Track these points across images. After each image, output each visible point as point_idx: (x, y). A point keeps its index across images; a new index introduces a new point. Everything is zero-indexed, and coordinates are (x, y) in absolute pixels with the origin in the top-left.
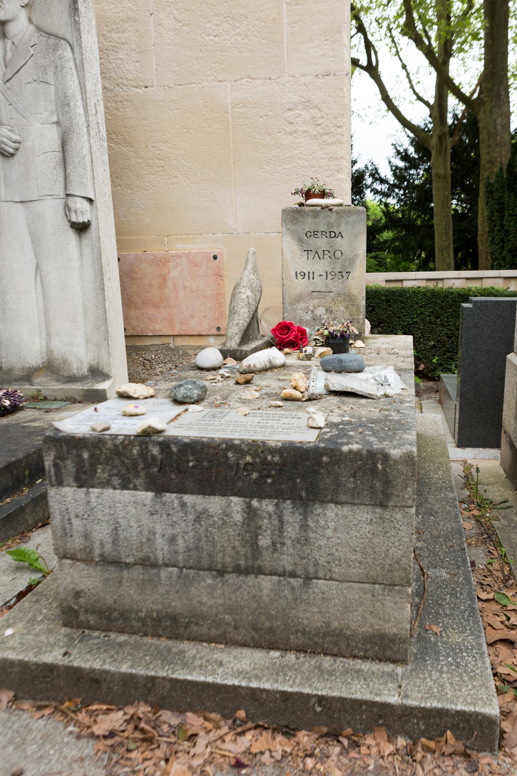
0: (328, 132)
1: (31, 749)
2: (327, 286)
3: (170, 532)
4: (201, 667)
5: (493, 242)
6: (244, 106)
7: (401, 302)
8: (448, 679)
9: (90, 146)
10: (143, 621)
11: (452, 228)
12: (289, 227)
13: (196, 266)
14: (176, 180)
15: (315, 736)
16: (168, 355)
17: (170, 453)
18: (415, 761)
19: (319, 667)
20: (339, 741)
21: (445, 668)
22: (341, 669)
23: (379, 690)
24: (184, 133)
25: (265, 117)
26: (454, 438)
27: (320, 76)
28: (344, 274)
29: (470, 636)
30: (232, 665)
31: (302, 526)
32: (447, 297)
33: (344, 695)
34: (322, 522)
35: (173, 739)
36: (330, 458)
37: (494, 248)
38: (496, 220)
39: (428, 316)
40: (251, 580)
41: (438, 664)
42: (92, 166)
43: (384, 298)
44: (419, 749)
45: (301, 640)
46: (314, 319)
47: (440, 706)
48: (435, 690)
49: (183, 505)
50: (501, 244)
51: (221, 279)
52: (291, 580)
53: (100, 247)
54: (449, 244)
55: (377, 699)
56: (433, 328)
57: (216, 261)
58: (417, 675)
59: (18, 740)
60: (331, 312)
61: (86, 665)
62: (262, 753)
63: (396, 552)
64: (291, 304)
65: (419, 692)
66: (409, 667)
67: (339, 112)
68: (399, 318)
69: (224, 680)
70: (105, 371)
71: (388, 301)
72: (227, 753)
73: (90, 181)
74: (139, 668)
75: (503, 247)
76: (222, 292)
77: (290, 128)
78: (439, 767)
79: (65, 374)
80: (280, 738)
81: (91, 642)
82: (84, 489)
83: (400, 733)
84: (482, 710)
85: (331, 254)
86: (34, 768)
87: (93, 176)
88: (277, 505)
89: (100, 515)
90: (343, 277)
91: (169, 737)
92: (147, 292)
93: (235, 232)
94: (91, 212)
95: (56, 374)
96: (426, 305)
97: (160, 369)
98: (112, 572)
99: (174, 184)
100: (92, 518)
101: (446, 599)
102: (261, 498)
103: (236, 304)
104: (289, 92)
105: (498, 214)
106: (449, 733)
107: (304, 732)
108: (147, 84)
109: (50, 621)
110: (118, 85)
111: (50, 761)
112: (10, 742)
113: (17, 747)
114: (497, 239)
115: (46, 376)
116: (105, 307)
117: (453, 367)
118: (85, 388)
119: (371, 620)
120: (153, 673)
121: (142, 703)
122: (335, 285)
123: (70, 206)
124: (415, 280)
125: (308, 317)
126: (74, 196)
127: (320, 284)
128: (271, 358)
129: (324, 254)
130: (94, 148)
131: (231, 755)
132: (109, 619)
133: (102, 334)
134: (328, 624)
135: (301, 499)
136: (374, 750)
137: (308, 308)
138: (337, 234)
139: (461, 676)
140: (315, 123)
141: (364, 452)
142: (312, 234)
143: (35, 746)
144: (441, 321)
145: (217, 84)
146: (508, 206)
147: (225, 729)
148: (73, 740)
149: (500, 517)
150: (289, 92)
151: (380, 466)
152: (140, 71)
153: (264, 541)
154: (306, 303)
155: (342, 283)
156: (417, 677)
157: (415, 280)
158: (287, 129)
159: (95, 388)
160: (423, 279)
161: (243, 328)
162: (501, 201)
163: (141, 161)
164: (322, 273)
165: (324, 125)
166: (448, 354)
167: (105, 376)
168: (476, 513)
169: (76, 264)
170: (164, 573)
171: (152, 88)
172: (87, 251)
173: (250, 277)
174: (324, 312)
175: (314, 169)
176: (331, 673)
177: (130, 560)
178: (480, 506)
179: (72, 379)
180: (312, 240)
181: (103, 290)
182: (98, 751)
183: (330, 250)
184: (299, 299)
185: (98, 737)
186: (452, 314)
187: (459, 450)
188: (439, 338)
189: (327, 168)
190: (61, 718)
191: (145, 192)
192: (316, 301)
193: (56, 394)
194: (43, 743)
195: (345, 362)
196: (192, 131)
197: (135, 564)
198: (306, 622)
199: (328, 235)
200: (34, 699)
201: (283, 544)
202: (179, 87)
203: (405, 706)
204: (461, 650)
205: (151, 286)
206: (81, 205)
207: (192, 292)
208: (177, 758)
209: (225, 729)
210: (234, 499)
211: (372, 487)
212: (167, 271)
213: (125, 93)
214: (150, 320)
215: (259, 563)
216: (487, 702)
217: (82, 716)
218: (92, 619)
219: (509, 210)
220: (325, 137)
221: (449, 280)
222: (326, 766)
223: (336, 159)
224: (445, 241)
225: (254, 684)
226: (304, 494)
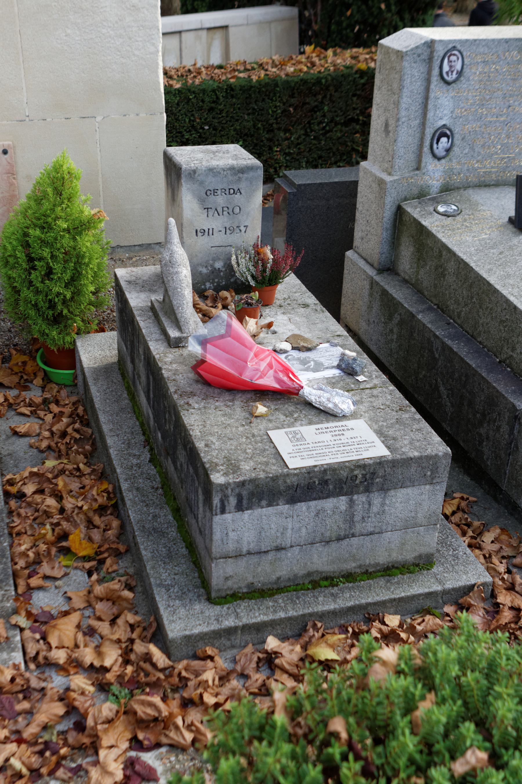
51: (14, 178)
57: (6, 156)
85: (230, 211)
90: (240, 231)
93: (27, 119)
129: (223, 211)
138: (236, 191)
142: (212, 192)
180: (212, 197)
183: (229, 206)
199: (227, 192)
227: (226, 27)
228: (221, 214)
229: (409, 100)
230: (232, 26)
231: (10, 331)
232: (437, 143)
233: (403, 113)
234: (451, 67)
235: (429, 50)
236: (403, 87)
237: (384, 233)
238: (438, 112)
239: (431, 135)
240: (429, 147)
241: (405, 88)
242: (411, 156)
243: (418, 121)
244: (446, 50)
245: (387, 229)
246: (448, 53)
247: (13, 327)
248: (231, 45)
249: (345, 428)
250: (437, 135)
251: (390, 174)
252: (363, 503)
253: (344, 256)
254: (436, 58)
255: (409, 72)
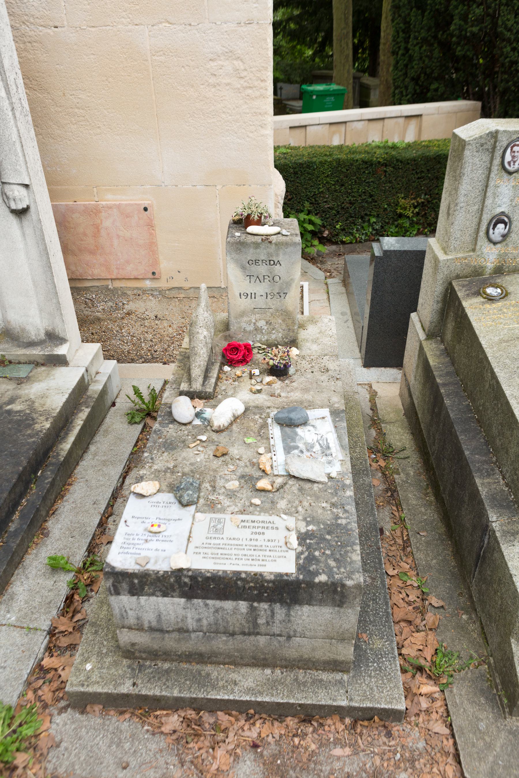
0: (251, 86)
1: (127, 746)
2: (267, 304)
3: (197, 617)
4: (223, 686)
5: (396, 67)
6: (164, 54)
7: (308, 173)
8: (376, 682)
9: (18, 130)
10: (179, 656)
11: (351, 9)
12: (233, 256)
13: (127, 217)
14: (99, 131)
15: (296, 720)
16: (108, 295)
17: (198, 582)
18: (356, 733)
19: (296, 680)
20: (312, 724)
21: (373, 674)
22: (310, 680)
23: (335, 696)
24: (103, 81)
25: (186, 67)
26: (360, 352)
27: (242, 24)
28: (282, 294)
29: (386, 642)
30: (243, 683)
31: (286, 615)
32: (352, 165)
33: (314, 703)
34: (300, 613)
35: (213, 733)
36: (307, 585)
37: (397, 74)
38: (401, 42)
39: (333, 185)
40: (252, 638)
41: (368, 670)
42: (23, 150)
43: (292, 171)
44: (359, 726)
45: (284, 663)
46: (256, 330)
47: (371, 705)
48: (368, 693)
49: (206, 605)
50: (404, 71)
52: (279, 638)
53: (41, 228)
54: (348, 33)
55: (335, 704)
56: (337, 196)
58: (357, 680)
59: (116, 740)
60: (270, 324)
61: (151, 693)
62: (268, 736)
63: (346, 626)
64: (236, 318)
65: (359, 695)
66: (351, 675)
67: (263, 65)
68: (306, 189)
69: (241, 697)
70: (61, 335)
71: (295, 173)
72: (247, 739)
73: (24, 167)
74: (185, 692)
75: (406, 74)
76: (155, 241)
77: (212, 80)
78: (370, 736)
79: (25, 341)
80: (276, 724)
81: (147, 671)
82: (136, 597)
83: (346, 716)
84: (396, 707)
85: (271, 279)
86: (134, 760)
87: (26, 161)
88: (270, 605)
89: (147, 609)
91: (210, 731)
92: (82, 240)
94: (29, 196)
95: (16, 340)
96: (332, 174)
97: (101, 307)
98: (157, 635)
99: (97, 134)
100: (142, 610)
101: (370, 606)
102: (259, 602)
103: (195, 345)
104: (210, 40)
105: (404, 35)
106: (376, 717)
107: (289, 718)
108: (57, 24)
109: (113, 653)
110: (23, 23)
111: (142, 754)
112: (112, 743)
113: (118, 746)
114: (401, 63)
115: (7, 342)
116: (54, 283)
117: (355, 231)
118: (46, 353)
119: (328, 654)
120: (195, 696)
121: (188, 708)
122: (274, 303)
123: (7, 194)
124: (319, 124)
125: (251, 328)
126: (9, 184)
127: (261, 302)
128: (234, 412)
130: (22, 131)
131: (250, 739)
132: (156, 655)
133: (54, 305)
134: (302, 656)
135: (287, 603)
136: (333, 727)
137: (250, 321)
139: (382, 680)
140: (238, 75)
141: (329, 583)
143: (128, 743)
144: (345, 188)
145: (133, 27)
146: (414, 27)
147: (242, 722)
148: (151, 736)
149: (400, 470)
150: (210, 40)
151: (339, 589)
152: (47, 8)
153: (261, 621)
154: (249, 317)
155: (280, 302)
156: (357, 683)
157: (319, 124)
158: (210, 81)
159: (55, 353)
160: (327, 124)
161: (204, 369)
162: (408, 20)
163: (60, 110)
164: (262, 294)
165: (248, 78)
166: (351, 219)
167: (62, 340)
168: (382, 463)
169: (21, 245)
170: (193, 635)
171: (63, 29)
172: (29, 231)
173: (205, 316)
174: (265, 324)
175: (238, 124)
176: (304, 684)
177: (171, 629)
178: (385, 457)
179: (31, 344)
180: (254, 268)
181: (50, 267)
182: (169, 744)
184: (243, 314)
185: (166, 734)
186: (355, 181)
187: (365, 370)
188: (343, 205)
189: (251, 123)
190: (137, 720)
191: (69, 142)
192: (257, 315)
193: (19, 358)
194: (133, 740)
195: (294, 420)
196: (110, 79)
197: (173, 631)
198: (287, 655)
199: (268, 263)
200: (116, 707)
201: (273, 622)
202: (93, 29)
203: (351, 707)
204: (381, 655)
205: (85, 235)
206: (18, 192)
207: (126, 240)
208: (219, 747)
209: (242, 722)
210: (241, 602)
211: (333, 598)
212: (99, 222)
213: (33, 32)
214: (87, 265)
215: (258, 630)
216: (398, 702)
217: (151, 719)
218: (144, 655)
219: (415, 32)
220: (249, 91)
221: (352, 123)
222: (306, 741)
223: (260, 114)
224: (344, 28)
225: (259, 699)
226: (288, 601)
227: (420, 116)
228: (262, 281)
229: (468, 186)
230: (425, 115)
231: (151, 341)
232: (494, 229)
233: (462, 199)
234: (513, 157)
235: (492, 141)
236: (464, 174)
237: (435, 305)
238: (497, 200)
239: (488, 221)
240: (484, 232)
241: (466, 175)
242: (468, 238)
243: (476, 207)
244: (510, 140)
245: (438, 302)
246: (511, 144)
247: (154, 338)
248: (423, 129)
249: (270, 525)
250: (494, 221)
251: (446, 253)
252: (265, 610)
253: (408, 317)
254: (498, 148)
255: (471, 161)
